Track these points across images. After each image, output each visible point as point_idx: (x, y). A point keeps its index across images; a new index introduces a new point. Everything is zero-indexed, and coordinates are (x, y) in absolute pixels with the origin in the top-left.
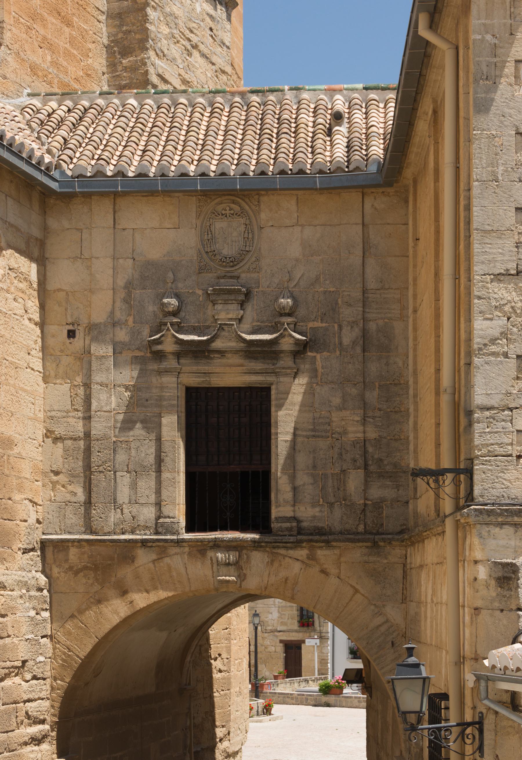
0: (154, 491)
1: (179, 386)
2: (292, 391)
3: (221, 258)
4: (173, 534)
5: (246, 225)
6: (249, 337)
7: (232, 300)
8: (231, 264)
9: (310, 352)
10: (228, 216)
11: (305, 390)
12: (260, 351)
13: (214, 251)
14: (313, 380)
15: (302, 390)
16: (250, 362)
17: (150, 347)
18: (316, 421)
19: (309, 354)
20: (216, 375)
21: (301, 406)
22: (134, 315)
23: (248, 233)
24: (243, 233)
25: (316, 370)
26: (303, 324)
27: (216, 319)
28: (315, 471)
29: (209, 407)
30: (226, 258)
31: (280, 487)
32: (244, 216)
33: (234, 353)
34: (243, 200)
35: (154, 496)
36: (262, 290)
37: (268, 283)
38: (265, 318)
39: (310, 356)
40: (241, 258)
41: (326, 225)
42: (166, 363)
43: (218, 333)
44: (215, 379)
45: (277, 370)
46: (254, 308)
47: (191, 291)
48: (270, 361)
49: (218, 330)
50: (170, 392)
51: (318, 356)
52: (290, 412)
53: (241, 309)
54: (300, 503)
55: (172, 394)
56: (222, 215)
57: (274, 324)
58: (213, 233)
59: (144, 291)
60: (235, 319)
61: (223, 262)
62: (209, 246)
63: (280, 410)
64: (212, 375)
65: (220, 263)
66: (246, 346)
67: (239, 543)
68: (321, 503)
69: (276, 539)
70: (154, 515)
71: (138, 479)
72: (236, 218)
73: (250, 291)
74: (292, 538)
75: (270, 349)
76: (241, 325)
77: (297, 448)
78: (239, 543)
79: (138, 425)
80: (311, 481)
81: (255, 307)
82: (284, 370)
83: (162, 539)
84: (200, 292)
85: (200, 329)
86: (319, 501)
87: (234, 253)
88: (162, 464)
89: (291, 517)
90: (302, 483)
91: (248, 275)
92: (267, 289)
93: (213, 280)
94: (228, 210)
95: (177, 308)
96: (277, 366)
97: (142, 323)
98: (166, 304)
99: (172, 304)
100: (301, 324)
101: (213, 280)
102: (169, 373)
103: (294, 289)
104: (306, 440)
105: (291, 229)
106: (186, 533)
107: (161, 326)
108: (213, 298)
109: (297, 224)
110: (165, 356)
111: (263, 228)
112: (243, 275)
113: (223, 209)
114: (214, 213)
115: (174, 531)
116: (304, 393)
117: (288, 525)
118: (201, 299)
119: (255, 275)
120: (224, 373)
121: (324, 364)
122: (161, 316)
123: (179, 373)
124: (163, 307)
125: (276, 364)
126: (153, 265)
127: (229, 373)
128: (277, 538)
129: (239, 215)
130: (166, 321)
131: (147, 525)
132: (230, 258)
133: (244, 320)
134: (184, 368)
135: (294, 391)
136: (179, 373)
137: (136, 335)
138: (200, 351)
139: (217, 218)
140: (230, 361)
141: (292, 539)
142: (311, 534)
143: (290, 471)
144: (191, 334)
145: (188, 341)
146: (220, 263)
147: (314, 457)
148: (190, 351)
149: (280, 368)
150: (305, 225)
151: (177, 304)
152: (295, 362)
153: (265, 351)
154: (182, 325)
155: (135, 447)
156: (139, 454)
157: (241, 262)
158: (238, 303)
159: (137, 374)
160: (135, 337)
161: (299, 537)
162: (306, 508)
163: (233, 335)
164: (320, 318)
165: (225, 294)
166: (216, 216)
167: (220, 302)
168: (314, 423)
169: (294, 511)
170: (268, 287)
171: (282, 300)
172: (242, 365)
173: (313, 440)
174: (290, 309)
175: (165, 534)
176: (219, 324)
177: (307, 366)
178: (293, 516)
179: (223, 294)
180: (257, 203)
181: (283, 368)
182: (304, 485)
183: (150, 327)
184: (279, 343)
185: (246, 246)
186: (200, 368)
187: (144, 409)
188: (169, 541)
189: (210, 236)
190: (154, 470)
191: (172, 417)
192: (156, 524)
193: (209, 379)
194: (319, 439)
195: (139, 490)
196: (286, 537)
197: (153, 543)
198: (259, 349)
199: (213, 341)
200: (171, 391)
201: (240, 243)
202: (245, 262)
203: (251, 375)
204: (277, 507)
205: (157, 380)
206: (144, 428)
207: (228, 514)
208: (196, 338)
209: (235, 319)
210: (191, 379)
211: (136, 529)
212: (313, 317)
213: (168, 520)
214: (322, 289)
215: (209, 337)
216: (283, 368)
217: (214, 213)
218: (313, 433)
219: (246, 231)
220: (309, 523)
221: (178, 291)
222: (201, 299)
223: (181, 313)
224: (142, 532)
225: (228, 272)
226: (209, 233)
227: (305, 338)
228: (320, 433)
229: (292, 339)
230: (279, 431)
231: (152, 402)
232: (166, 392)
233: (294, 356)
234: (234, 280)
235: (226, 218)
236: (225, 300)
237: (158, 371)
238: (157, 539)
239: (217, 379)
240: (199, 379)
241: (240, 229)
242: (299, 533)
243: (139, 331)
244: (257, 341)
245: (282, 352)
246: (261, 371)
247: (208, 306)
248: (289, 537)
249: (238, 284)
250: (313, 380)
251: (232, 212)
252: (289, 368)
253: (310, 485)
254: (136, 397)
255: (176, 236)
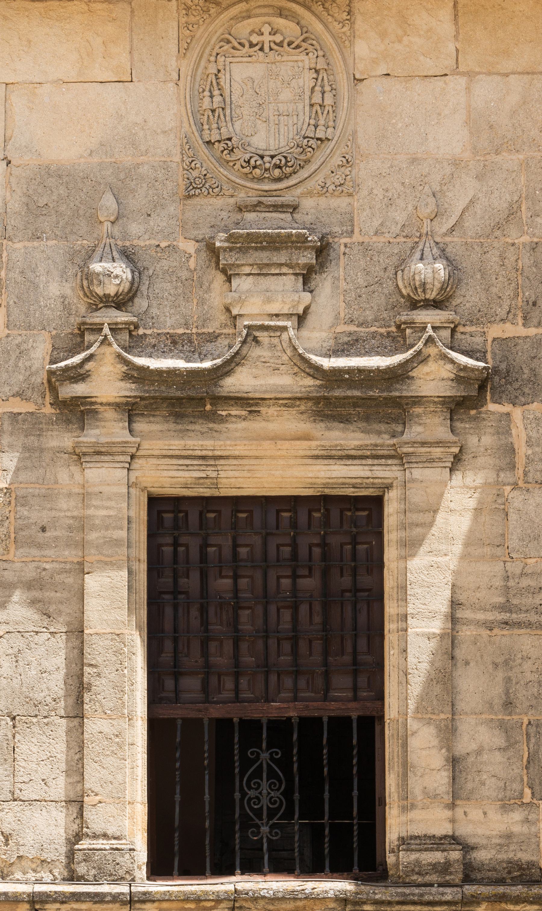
0: (63, 767)
1: (132, 490)
2: (445, 503)
3: (247, 156)
4: (118, 880)
5: (317, 71)
6: (327, 363)
7: (281, 265)
8: (277, 172)
9: (495, 402)
10: (267, 49)
11: (480, 502)
12: (358, 398)
13: (230, 139)
14: (502, 475)
15: (472, 503)
16: (328, 429)
17: (53, 389)
18: (511, 583)
19: (492, 407)
20: (235, 462)
21: (467, 545)
22: (8, 307)
23: (323, 93)
24: (308, 93)
25: (512, 450)
26: (473, 329)
27: (235, 318)
28: (510, 714)
29: (209, 549)
30: (262, 157)
31: (412, 758)
32: (310, 48)
33: (285, 405)
34: (308, 8)
35: (62, 780)
36: (361, 240)
37: (376, 223)
38: (370, 315)
39: (493, 413)
40: (302, 157)
41: (533, 73)
42: (97, 431)
43: (244, 352)
44: (231, 474)
45: (405, 450)
46: (338, 287)
47: (163, 244)
48: (383, 427)
49: (244, 342)
50: (107, 508)
51: (517, 413)
52: (440, 559)
53: (304, 290)
54: (468, 799)
55: (112, 513)
56: (252, 45)
57: (393, 329)
58: (227, 93)
59: (36, 244)
60: (289, 316)
61: (254, 167)
62: (215, 126)
63: (413, 555)
64: (222, 462)
65: (247, 170)
66: (320, 386)
67: (300, 904)
68: (527, 797)
69: (404, 894)
70: (62, 831)
71: (18, 737)
72: (288, 54)
73: (328, 244)
74: (448, 890)
75: (385, 394)
76: (305, 333)
77: (460, 653)
78: (300, 904)
79: (17, 596)
80: (499, 740)
81: (343, 285)
82: (423, 450)
83: (88, 894)
84: (190, 247)
85: (190, 342)
86: (521, 795)
87: (283, 144)
88: (87, 697)
89: (445, 837)
90: (474, 746)
91: (323, 202)
92: (375, 239)
93: (224, 214)
94: (266, 33)
95: (127, 285)
96: (406, 437)
97: (29, 327)
98: (98, 274)
99: (117, 277)
100: (468, 329)
101: (224, 214)
102: (106, 458)
103: (448, 239)
104: (485, 633)
105: (439, 83)
106: (148, 879)
107: (82, 335)
108: (225, 259)
109: (456, 71)
110: (96, 412)
111: (361, 80)
112: (308, 204)
113: (253, 32)
114: (228, 42)
115: (121, 872)
116: (478, 511)
117: (438, 857)
118: (192, 264)
119: (342, 203)
120: (257, 458)
121: (534, 434)
122: (83, 309)
123: (133, 457)
124: (91, 283)
125: (402, 433)
126: (60, 177)
127: (272, 457)
128: (407, 891)
129: (298, 47)
130: (97, 320)
131: (44, 856)
132: (272, 157)
133: (311, 320)
134: (145, 445)
135: (452, 505)
136: (133, 457)
137: (13, 357)
138: (191, 399)
139: (237, 53)
140: (274, 427)
141: (449, 894)
142: (501, 882)
143: (442, 716)
144: (164, 354)
145: (159, 372)
146: (247, 170)
147: (508, 680)
148: (165, 399)
149: (413, 443)
150: (479, 73)
151: (130, 276)
152: (453, 430)
153: (370, 398)
154: (141, 331)
155: (10, 651)
156: (21, 670)
157: (302, 167)
158: (296, 274)
159: (16, 460)
160: (11, 363)
161: (470, 889)
162: (485, 813)
163: (285, 358)
164: (521, 314)
165: (263, 249)
166: (234, 48)
167: (247, 270)
168: (507, 588)
169: (453, 821)
170: (376, 234)
171: (420, 266)
172: (307, 437)
173: (505, 632)
174: (442, 289)
175: (96, 881)
176: (245, 327)
177: (487, 440)
178: (450, 833)
179: (256, 249)
180: (345, 16)
181: (423, 444)
182: (479, 752)
183: (52, 337)
184: (409, 378)
185: (316, 126)
186: (190, 443)
187: (34, 552)
188: (109, 898)
189: (217, 99)
190: (63, 713)
191: (113, 574)
192: (71, 855)
193: (214, 475)
194: (522, 631)
195: (23, 764)
196: (434, 890)
197: (63, 902)
198: (357, 393)
199: (228, 373)
200: (113, 504)
201: (301, 117)
202: (312, 167)
203: (331, 461)
204: (404, 809)
205: (72, 476)
206: (33, 602)
207: (265, 829)
208: (180, 364)
209: (289, 316)
210: (165, 473)
211: (14, 868)
212: (502, 312)
213: (100, 843)
214: (526, 239)
215: (218, 361)
216: (423, 444)
217: (228, 42)
218: (505, 616)
219: (318, 88)
220: (493, 852)
221: (128, 244)
222: (192, 264)
223: (136, 300)
224: (31, 876)
225: (268, 193)
226: (216, 92)
227: (482, 364)
228: (522, 617)
229: (449, 366)
230: (410, 611)
231: (58, 533)
232: (96, 507)
233: (452, 412)
234: (282, 216)
235: (261, 53)
236: (261, 266)
237: (74, 453)
238: (73, 894)
239: (237, 474)
240: (187, 474)
241: (301, 82)
242: (467, 879)
243: (24, 347)
244: (350, 371)
245: (418, 401)
246: (360, 453)
247: (211, 282)
248: (441, 889)
249: (296, 225)
250: (502, 475)
251: (278, 38)
252: (438, 443)
253: (497, 753)
254: (12, 519)
255: (125, 102)
